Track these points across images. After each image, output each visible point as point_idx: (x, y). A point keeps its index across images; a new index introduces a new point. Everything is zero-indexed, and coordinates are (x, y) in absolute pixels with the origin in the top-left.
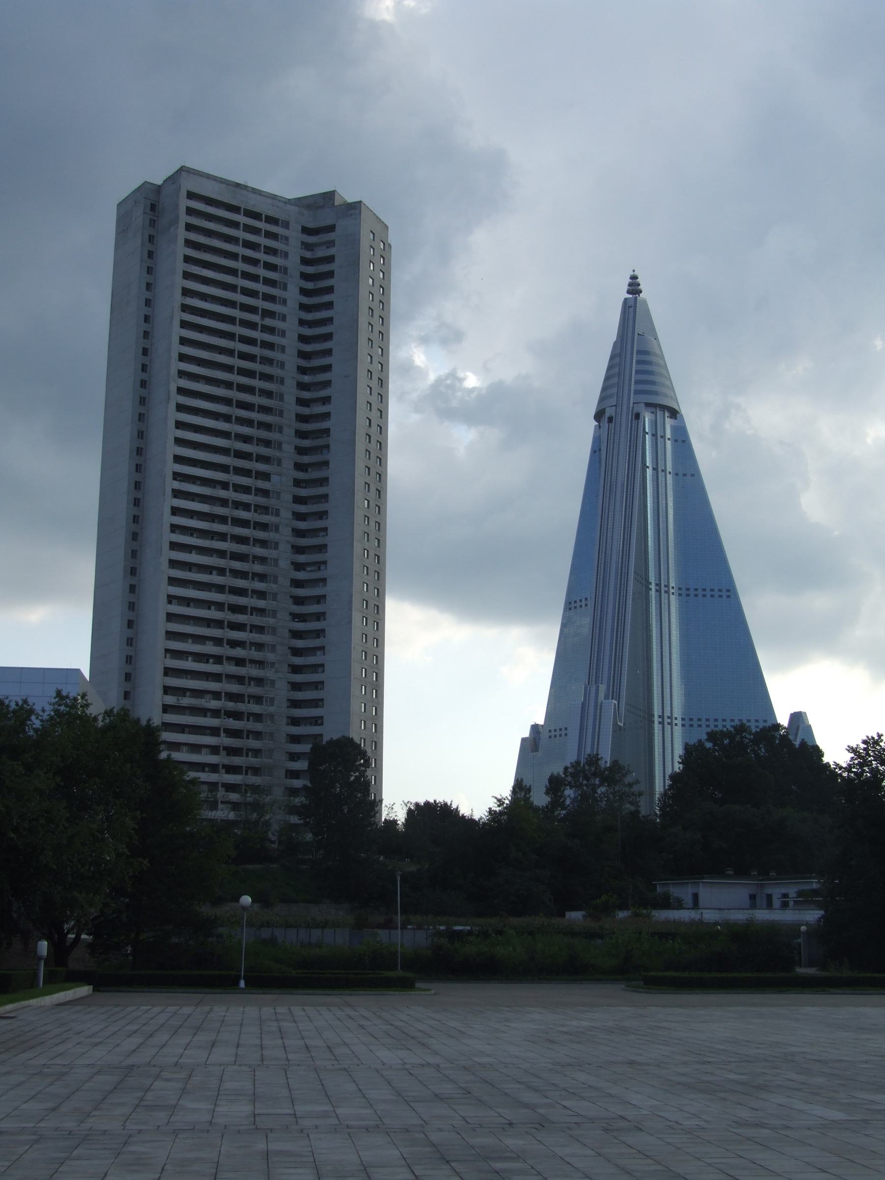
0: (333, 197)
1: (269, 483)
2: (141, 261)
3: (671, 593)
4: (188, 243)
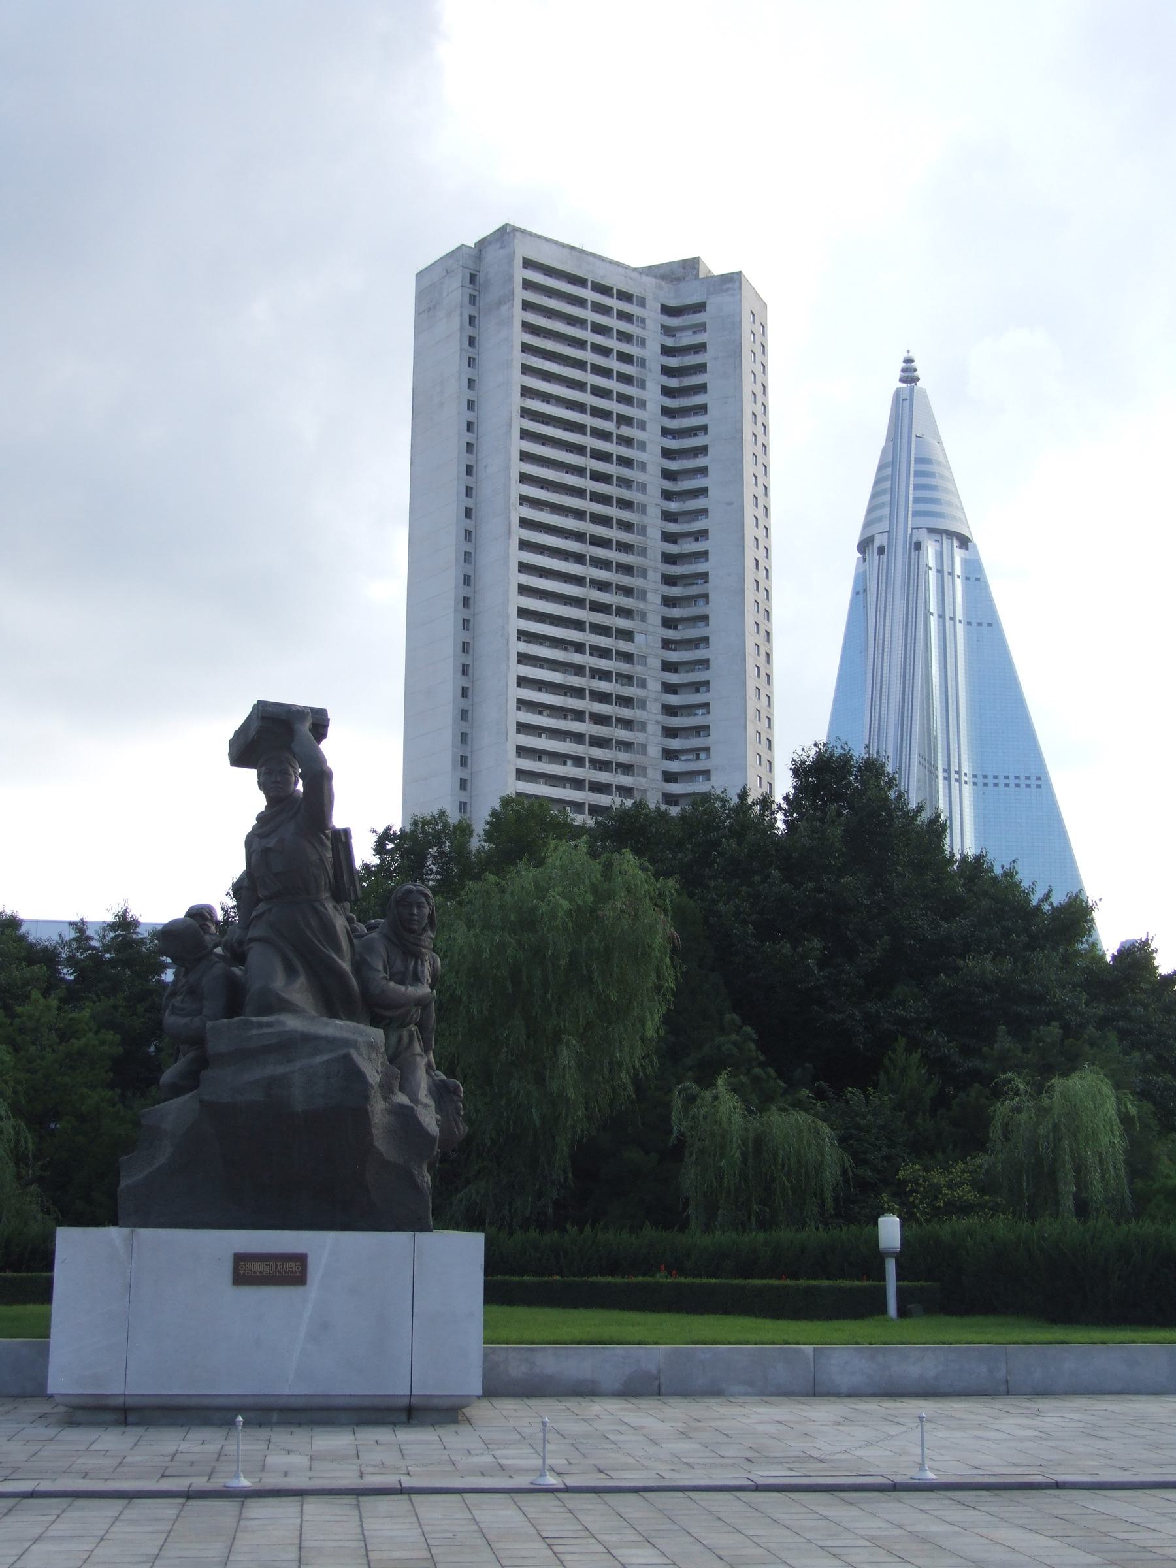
0: (697, 266)
1: (633, 644)
2: (461, 350)
3: (963, 782)
4: (528, 327)
